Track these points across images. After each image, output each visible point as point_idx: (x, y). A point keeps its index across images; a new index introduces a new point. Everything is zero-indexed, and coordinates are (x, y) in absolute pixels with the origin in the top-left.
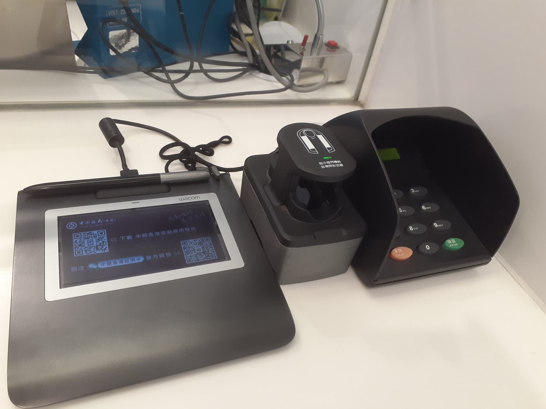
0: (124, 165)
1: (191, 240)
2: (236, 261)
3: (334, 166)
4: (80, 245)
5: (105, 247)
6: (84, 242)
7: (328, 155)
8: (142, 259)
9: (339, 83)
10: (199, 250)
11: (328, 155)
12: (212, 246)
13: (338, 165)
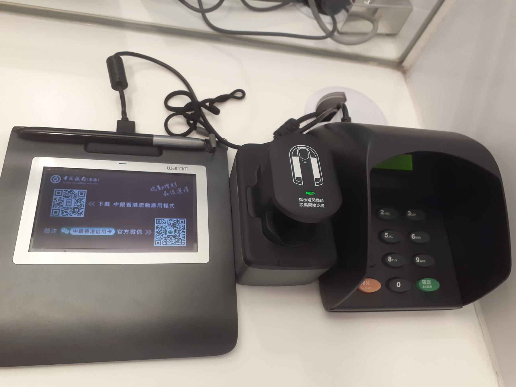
0: (124, 113)
1: (166, 220)
2: (201, 255)
3: (314, 205)
4: (59, 204)
5: (81, 211)
6: (63, 201)
7: (312, 188)
8: (113, 232)
9: (391, 35)
10: (170, 232)
11: (312, 188)
12: (185, 230)
13: (318, 206)
